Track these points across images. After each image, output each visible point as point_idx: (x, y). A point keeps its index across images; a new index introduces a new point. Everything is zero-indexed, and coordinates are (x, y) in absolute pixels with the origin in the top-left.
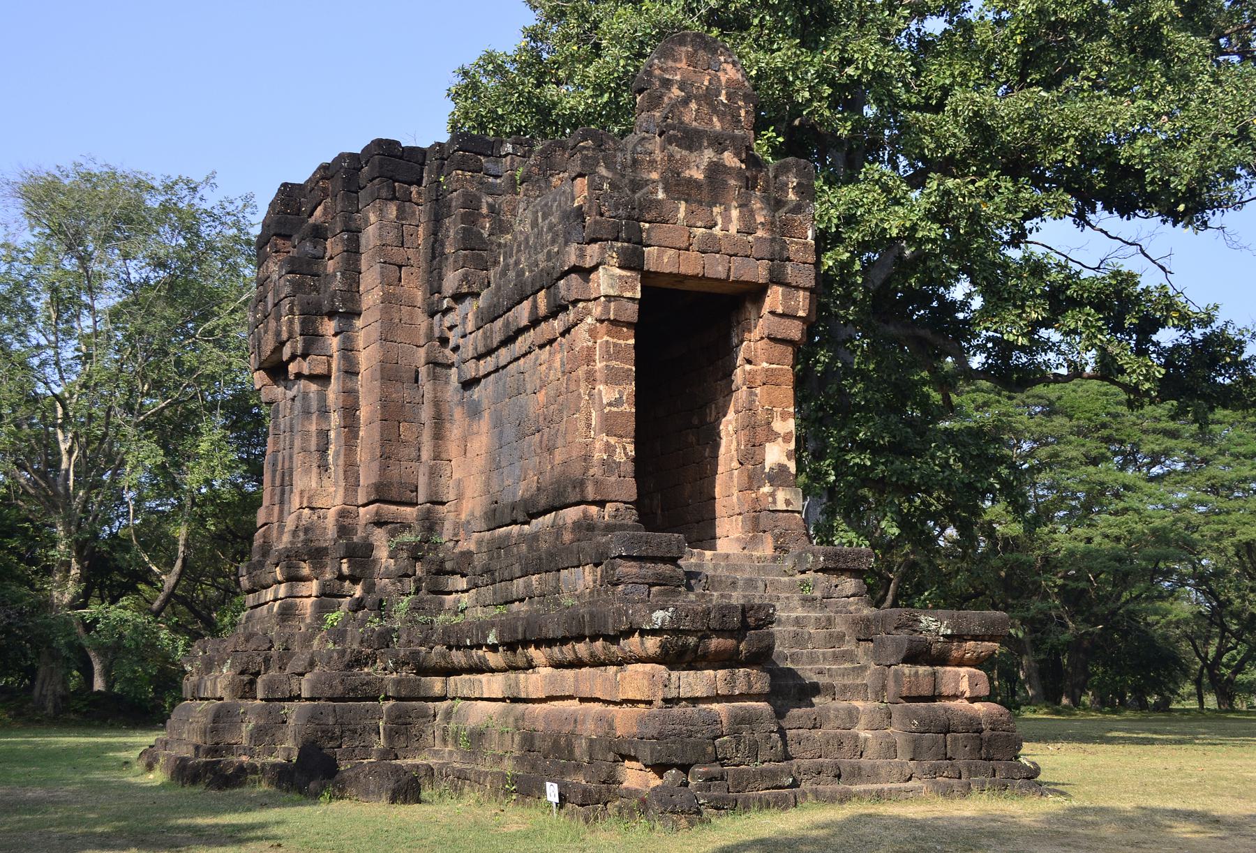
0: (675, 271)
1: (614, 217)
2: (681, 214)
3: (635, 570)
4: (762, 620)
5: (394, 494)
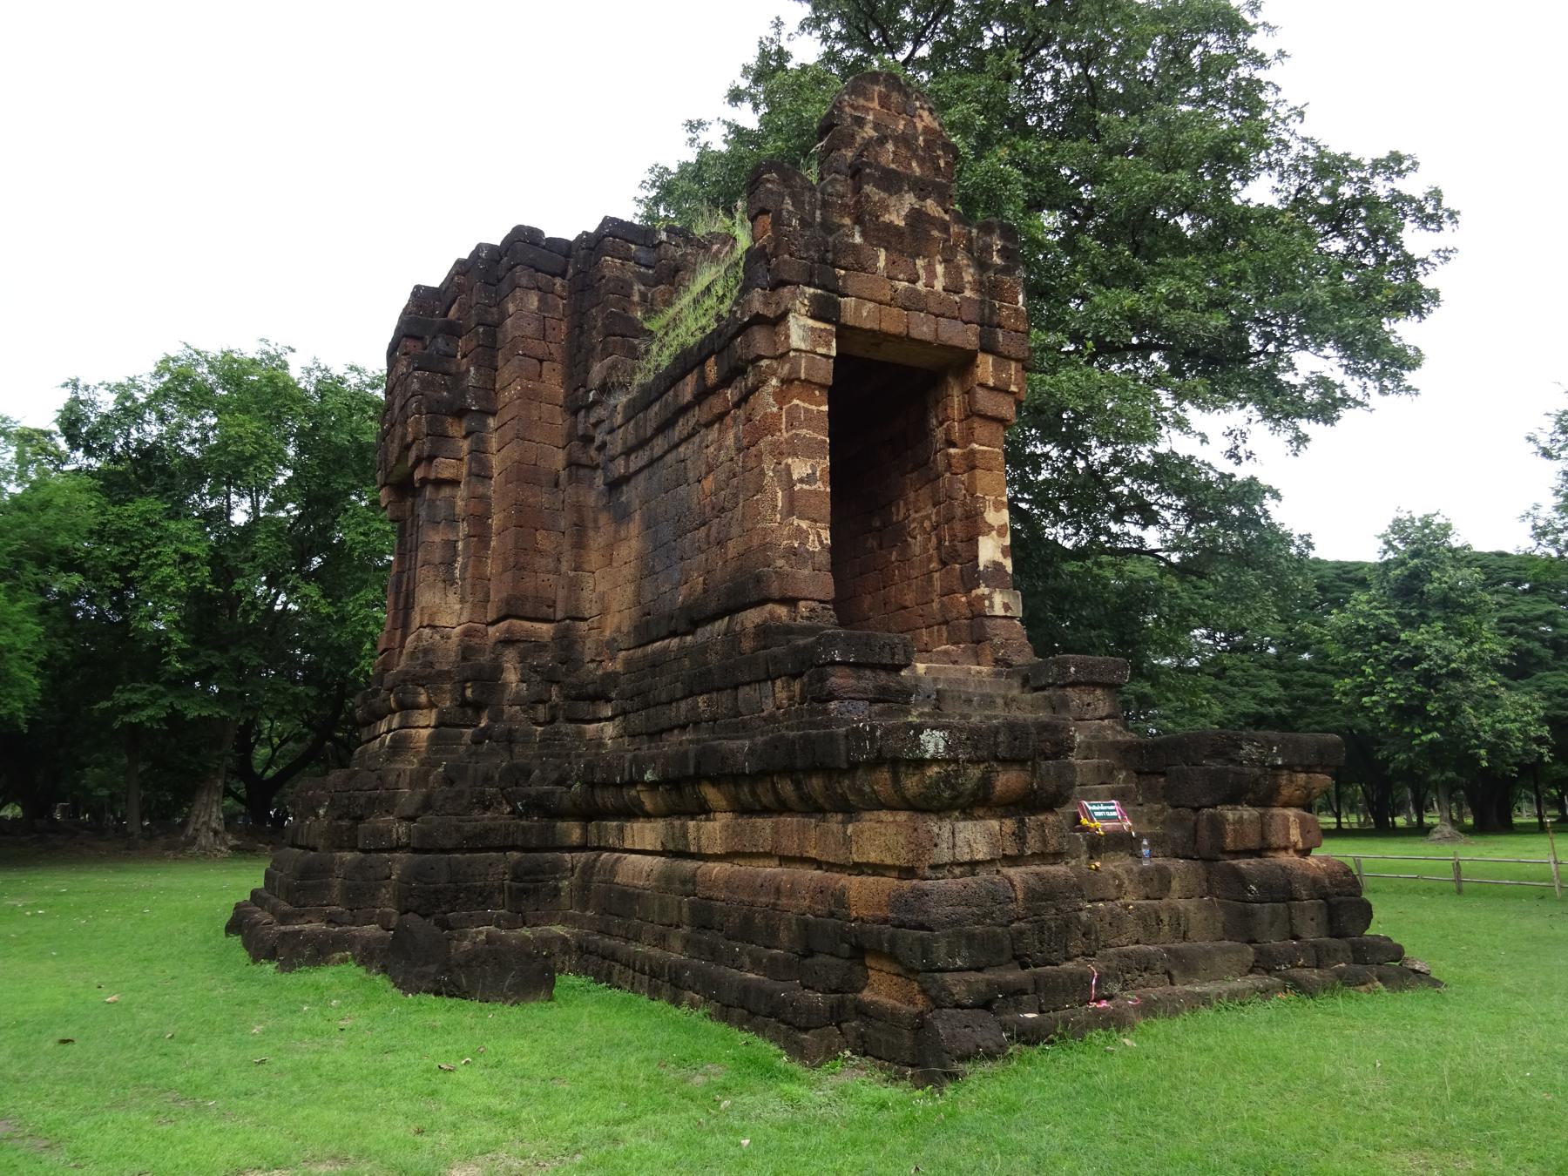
0: (876, 327)
2: (882, 263)
5: (528, 609)
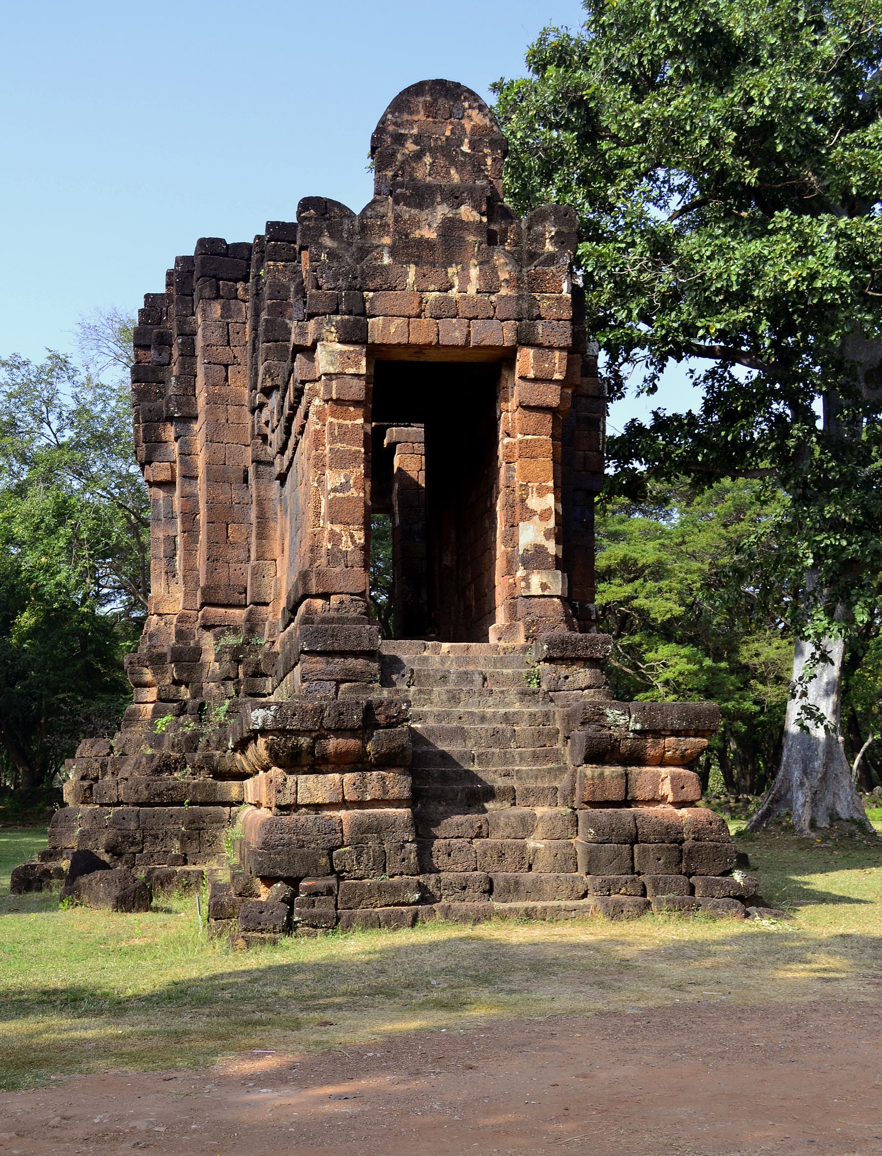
0: (404, 340)
1: (333, 289)
3: (320, 666)
4: (394, 717)
5: (221, 597)
